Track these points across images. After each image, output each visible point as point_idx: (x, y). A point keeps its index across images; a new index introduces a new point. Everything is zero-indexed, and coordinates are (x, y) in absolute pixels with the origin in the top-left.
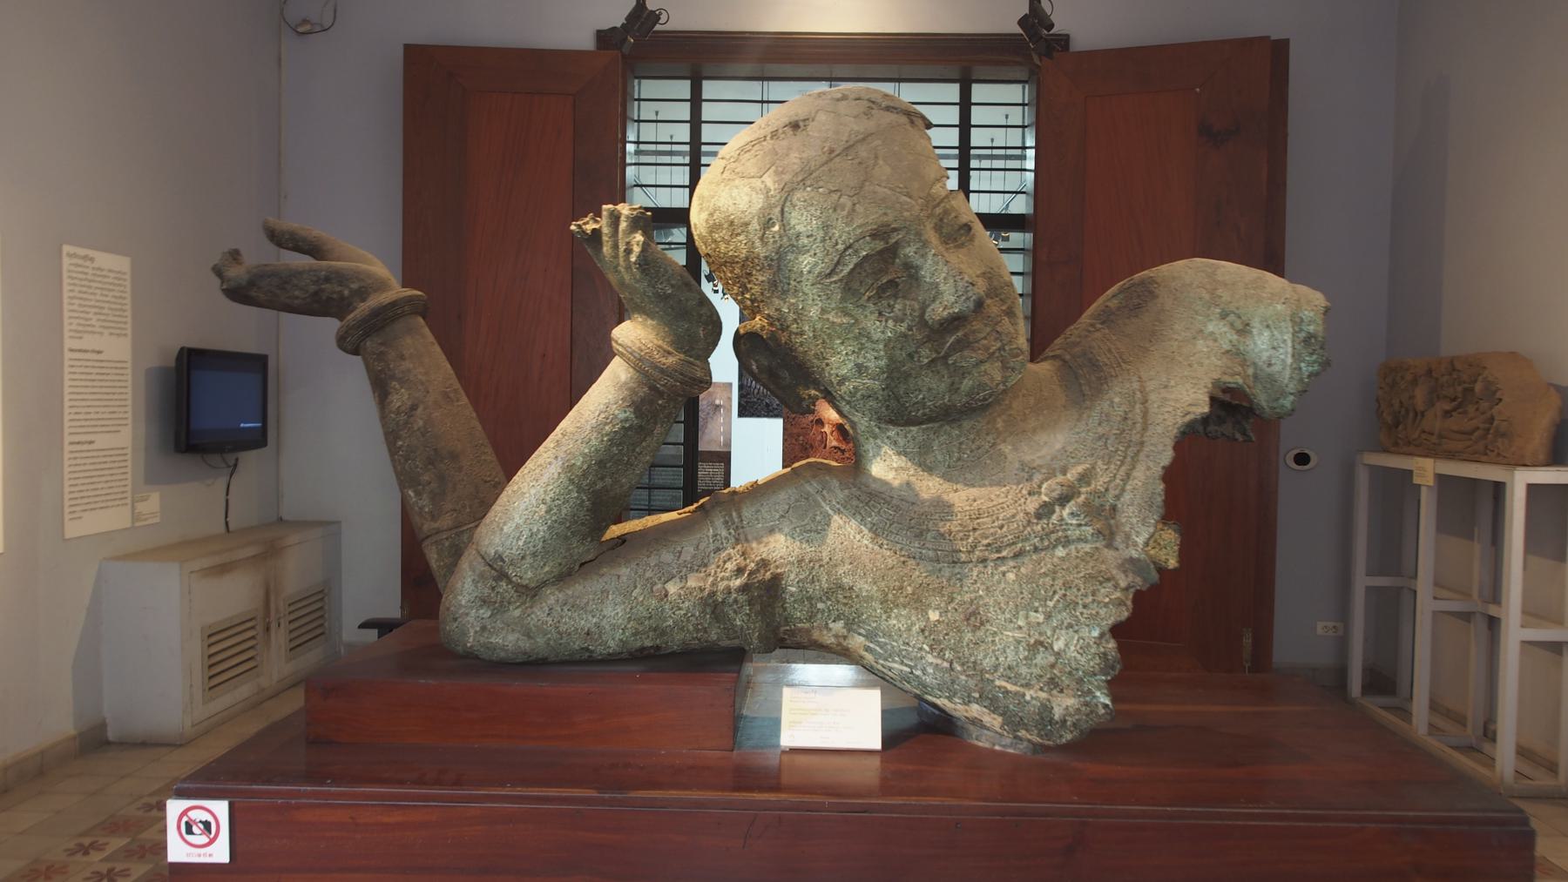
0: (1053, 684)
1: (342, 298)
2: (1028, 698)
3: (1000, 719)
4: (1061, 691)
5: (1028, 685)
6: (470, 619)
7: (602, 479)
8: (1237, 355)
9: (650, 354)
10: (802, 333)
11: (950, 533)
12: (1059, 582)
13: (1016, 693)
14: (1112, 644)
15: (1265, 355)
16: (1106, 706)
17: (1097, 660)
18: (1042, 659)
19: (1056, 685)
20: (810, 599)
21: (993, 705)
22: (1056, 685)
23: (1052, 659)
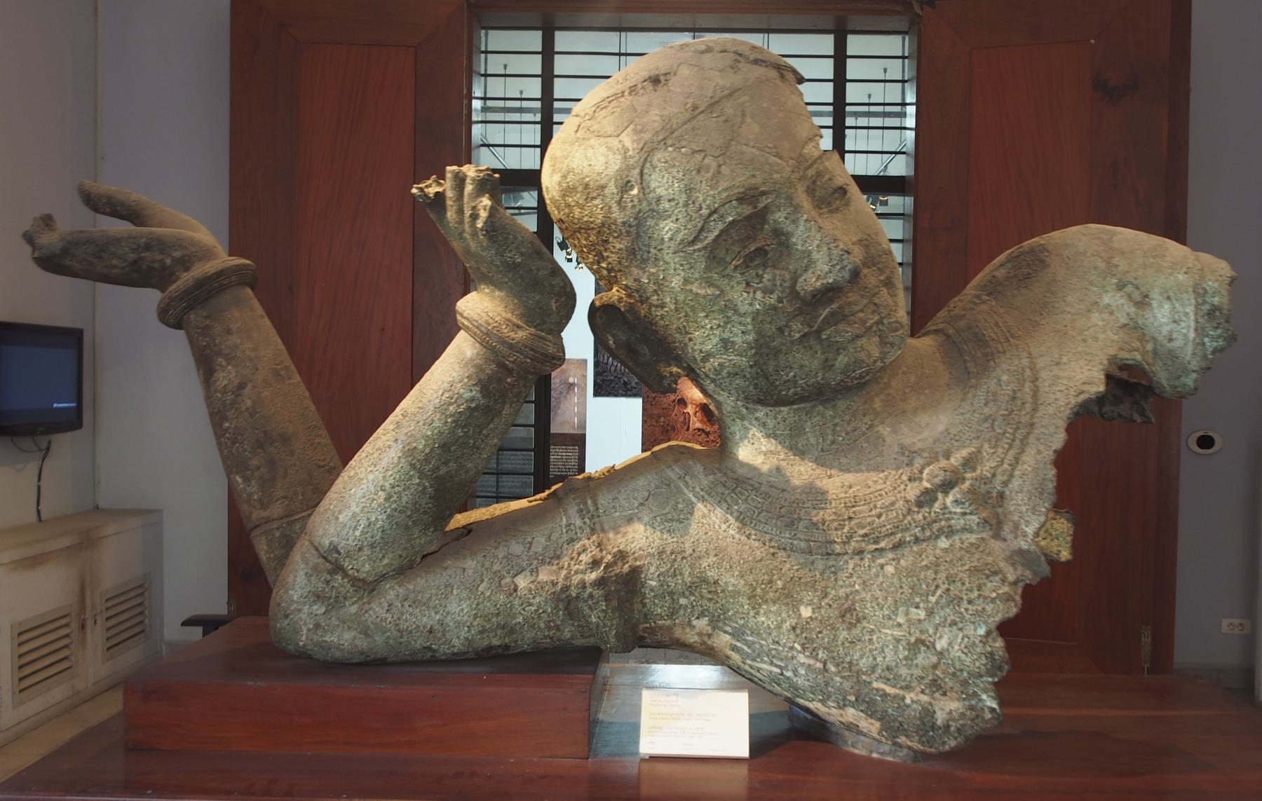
0: (935, 686)
1: (164, 267)
2: (908, 701)
5: (908, 688)
7: (446, 463)
12: (942, 575)
13: (895, 696)
14: (999, 643)
16: (992, 710)
19: (939, 688)
20: (671, 593)
22: (939, 688)
23: (934, 659)
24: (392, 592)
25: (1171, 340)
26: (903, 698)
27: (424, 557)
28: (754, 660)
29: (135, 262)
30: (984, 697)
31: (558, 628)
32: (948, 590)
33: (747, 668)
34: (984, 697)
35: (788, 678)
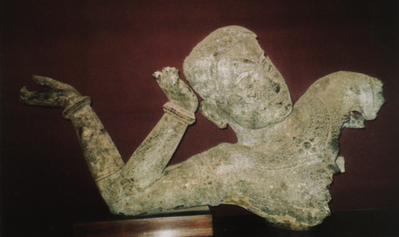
0: (311, 205)
1: (66, 101)
2: (303, 211)
3: (295, 219)
4: (314, 207)
5: (303, 207)
6: (123, 201)
7: (164, 152)
8: (357, 102)
9: (332, 139)
10: (223, 103)
11: (255, 81)
12: (309, 173)
13: (299, 210)
14: (328, 191)
15: (365, 100)
16: (328, 211)
17: (324, 196)
18: (306, 197)
19: (312, 206)
20: (231, 185)
21: (292, 213)
22: (312, 206)
23: (310, 197)
24: (374, 91)
25: (330, 178)
26: (302, 210)
27: (156, 180)
28: (256, 204)
29: (57, 99)
30: (325, 207)
31: (198, 199)
32: (311, 177)
33: (254, 207)
34: (325, 207)
35: (267, 208)
